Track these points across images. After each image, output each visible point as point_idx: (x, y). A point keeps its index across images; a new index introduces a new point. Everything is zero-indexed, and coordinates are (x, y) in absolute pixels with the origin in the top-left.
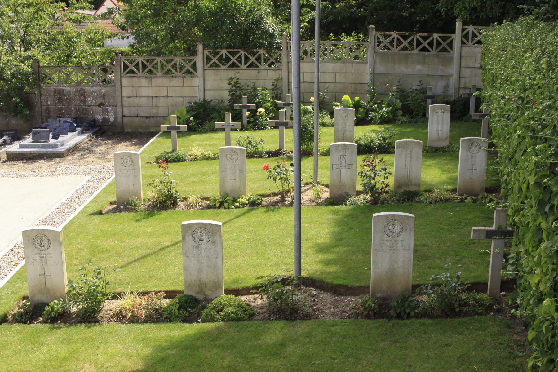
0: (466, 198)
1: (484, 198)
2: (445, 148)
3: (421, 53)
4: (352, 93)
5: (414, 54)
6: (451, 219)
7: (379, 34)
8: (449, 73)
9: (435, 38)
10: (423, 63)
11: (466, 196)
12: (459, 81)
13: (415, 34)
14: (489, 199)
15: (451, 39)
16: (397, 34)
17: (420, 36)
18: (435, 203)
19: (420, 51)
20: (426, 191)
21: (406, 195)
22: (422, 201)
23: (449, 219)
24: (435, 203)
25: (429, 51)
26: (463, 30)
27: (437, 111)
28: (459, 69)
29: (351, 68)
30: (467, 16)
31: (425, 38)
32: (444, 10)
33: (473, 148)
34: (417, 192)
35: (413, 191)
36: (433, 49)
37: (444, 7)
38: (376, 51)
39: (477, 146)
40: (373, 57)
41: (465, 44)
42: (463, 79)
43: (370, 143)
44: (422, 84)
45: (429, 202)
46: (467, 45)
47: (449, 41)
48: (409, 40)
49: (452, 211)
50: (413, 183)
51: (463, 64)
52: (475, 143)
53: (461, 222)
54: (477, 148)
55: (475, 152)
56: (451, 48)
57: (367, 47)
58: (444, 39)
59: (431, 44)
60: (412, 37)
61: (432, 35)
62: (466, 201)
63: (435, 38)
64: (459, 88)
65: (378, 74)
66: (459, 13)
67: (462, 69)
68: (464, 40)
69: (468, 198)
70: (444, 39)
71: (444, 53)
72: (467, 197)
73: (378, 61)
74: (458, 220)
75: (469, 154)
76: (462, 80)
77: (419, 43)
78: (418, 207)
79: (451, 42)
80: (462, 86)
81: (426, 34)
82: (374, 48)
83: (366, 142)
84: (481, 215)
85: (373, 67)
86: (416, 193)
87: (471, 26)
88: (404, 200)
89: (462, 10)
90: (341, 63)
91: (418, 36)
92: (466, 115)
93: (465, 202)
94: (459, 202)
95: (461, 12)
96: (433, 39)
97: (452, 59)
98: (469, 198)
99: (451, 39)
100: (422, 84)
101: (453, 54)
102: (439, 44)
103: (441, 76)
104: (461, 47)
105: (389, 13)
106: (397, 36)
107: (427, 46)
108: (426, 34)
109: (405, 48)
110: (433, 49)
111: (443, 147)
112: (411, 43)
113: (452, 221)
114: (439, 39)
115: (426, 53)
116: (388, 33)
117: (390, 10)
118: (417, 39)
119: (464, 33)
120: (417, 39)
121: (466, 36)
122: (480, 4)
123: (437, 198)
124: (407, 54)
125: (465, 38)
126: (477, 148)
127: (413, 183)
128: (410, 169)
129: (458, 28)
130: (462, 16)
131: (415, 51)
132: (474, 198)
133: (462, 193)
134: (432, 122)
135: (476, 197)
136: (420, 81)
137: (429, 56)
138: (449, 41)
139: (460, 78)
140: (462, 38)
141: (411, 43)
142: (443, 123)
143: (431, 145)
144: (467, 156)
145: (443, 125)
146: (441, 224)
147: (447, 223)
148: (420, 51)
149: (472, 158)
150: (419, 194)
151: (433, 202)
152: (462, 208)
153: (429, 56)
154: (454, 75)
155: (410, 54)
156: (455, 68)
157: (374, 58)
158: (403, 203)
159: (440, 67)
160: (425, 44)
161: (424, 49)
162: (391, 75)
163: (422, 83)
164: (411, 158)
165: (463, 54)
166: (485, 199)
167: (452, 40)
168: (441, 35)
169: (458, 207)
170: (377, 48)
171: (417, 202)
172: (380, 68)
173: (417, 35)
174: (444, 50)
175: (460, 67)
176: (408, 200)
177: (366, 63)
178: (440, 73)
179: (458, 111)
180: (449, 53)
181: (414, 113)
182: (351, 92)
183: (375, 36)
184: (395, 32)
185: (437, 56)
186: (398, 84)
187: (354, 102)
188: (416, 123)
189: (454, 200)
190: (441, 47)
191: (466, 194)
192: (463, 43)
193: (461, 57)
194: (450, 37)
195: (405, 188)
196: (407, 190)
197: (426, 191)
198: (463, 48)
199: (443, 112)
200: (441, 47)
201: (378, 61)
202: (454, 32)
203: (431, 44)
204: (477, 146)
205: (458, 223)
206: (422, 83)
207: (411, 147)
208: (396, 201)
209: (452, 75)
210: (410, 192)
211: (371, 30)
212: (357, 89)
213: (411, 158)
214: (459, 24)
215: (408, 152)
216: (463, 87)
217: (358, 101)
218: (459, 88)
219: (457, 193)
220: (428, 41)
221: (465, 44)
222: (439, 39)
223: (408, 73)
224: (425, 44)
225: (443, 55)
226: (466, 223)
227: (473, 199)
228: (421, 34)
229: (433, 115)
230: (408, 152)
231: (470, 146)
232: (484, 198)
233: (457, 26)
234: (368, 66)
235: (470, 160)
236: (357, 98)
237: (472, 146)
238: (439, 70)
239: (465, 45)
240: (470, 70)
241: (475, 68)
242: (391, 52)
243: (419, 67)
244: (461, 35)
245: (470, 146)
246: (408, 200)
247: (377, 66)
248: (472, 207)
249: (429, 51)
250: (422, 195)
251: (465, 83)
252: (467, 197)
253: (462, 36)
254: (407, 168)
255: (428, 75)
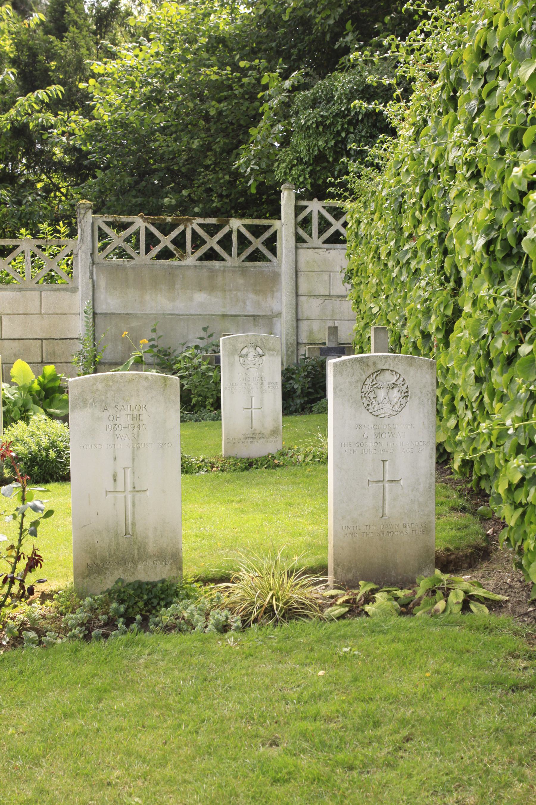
0: (369, 599)
1: (439, 593)
2: (274, 458)
3: (205, 263)
4: (42, 362)
5: (188, 267)
6: (324, 708)
7: (101, 220)
8: (272, 310)
9: (235, 228)
10: (212, 288)
11: (371, 586)
12: (297, 327)
13: (188, 220)
14: (462, 597)
15: (271, 232)
16: (145, 220)
17: (200, 225)
18: (245, 624)
19: (201, 259)
20: (206, 581)
21: (122, 601)
22: (188, 622)
23: (312, 709)
24: (245, 624)
25: (223, 260)
26: (299, 209)
27: (244, 352)
28: (294, 300)
29: (37, 303)
30: (305, 179)
31: (211, 230)
32: (252, 169)
33: (382, 394)
34: (169, 587)
35: (154, 585)
36: (230, 255)
37: (253, 162)
38: (97, 260)
39: (394, 386)
40: (91, 274)
41: (304, 241)
42: (305, 322)
43: (47, 450)
44: (211, 336)
45: (216, 626)
46: (309, 245)
47: (267, 235)
48: (174, 234)
49: (322, 662)
50: (151, 548)
51: (303, 288)
52: (387, 374)
53: (377, 724)
54: (395, 394)
55: (388, 409)
56: (273, 251)
57: (74, 252)
58: (257, 231)
59: (225, 243)
60: (181, 228)
61: (228, 222)
62: (367, 608)
63: (235, 228)
64: (298, 344)
65: (106, 314)
66: (285, 173)
67: (302, 299)
68: (301, 232)
69: (378, 596)
70: (257, 231)
71: (257, 264)
72: (373, 591)
73: (102, 283)
74: (360, 707)
75: (368, 420)
76: (304, 326)
77: (198, 242)
78: (166, 653)
79: (273, 238)
80: (303, 338)
81: (213, 221)
82: (92, 254)
83: (34, 448)
84: (460, 671)
85: (91, 298)
86: (163, 591)
87: (316, 200)
88: (111, 624)
89: (294, 166)
90: (14, 290)
91: (196, 224)
92: (319, 399)
93: (367, 614)
94: (342, 617)
95: (291, 169)
96: (230, 233)
97: (275, 277)
98: (380, 596)
99: (271, 232)
100: (211, 336)
101: (279, 265)
102: (243, 242)
103: (255, 317)
104: (297, 248)
105: (134, 201)
106: (146, 224)
107: (172, 247)
108: (213, 221)
109: (165, 254)
110: (230, 255)
111: (266, 457)
112: (179, 242)
113: (328, 720)
114: (244, 230)
115: (217, 264)
116: (124, 219)
117: (135, 197)
118: (194, 232)
119: (301, 217)
120: (194, 232)
121: (306, 223)
122: (332, 143)
123: (252, 604)
124: (172, 267)
125: (304, 228)
126: (395, 394)
127: (151, 548)
128: (134, 490)
129: (286, 204)
130: (293, 180)
131: (191, 260)
132: (400, 593)
133: (350, 576)
134: (232, 385)
135: (407, 592)
136: (205, 329)
137: (224, 271)
138: (267, 235)
139: (297, 320)
140: (296, 228)
141: (179, 242)
142: (262, 387)
143: (233, 453)
144: (359, 426)
145: (262, 392)
146: (274, 743)
147: (304, 735)
148: (201, 259)
149: (378, 435)
150: (177, 594)
151: (236, 621)
152: (360, 641)
153: (224, 271)
154: (284, 313)
155: (179, 267)
156: (284, 298)
157: (92, 278)
158: (106, 636)
159: (251, 296)
160: (213, 242)
161: (211, 255)
162: (136, 316)
163: (209, 332)
164: (136, 447)
165: (302, 266)
166: (446, 595)
167: (275, 233)
168: (248, 221)
169: (345, 637)
170: (102, 255)
171: (168, 629)
172: (109, 301)
173: (192, 223)
174: (256, 256)
175: (297, 295)
176: (129, 621)
177: (74, 290)
178: (250, 310)
179: (299, 391)
180: (268, 264)
181: (194, 401)
182: (40, 360)
183: (93, 225)
184: (142, 217)
185: (243, 271)
186: (154, 336)
187: (44, 377)
188: (196, 421)
189: (322, 608)
190: (249, 251)
191: (368, 580)
192: (299, 240)
193: (297, 272)
194: (269, 227)
195: (119, 574)
196: (130, 579)
197: (206, 581)
198: (301, 251)
199: (261, 356)
200: (249, 251)
201: (102, 283)
202: (276, 213)
203: (225, 243)
204: (394, 386)
205: (359, 729)
206: (209, 332)
207: (133, 402)
208: (76, 631)
209: (279, 315)
210: (139, 586)
211: (83, 211)
212: (54, 354)
213: (136, 447)
214: (289, 195)
215: (123, 420)
216: (305, 341)
217: (54, 378)
218: (298, 344)
219: (330, 578)
220: (220, 235)
221: (304, 241)
222: (244, 230)
223: (177, 312)
224: (213, 242)
225: (255, 267)
226: (404, 722)
227: (396, 599)
228: (200, 220)
229: (231, 365)
230: (123, 420)
231: (366, 389)
232: (439, 593)
233: (283, 202)
234: (79, 295)
235: (371, 444)
236: (49, 369)
237: (375, 387)
238: (248, 303)
239: (305, 245)
240: (319, 301)
241: (329, 296)
242: (133, 262)
243: (200, 297)
244: (293, 221)
245: (366, 389)
246: (129, 621)
247: (102, 295)
248: (404, 635)
249: (223, 260)
250: (188, 596)
251: (311, 332)
252: (373, 591)
253: (296, 224)
254: (120, 487)
255: (224, 316)
